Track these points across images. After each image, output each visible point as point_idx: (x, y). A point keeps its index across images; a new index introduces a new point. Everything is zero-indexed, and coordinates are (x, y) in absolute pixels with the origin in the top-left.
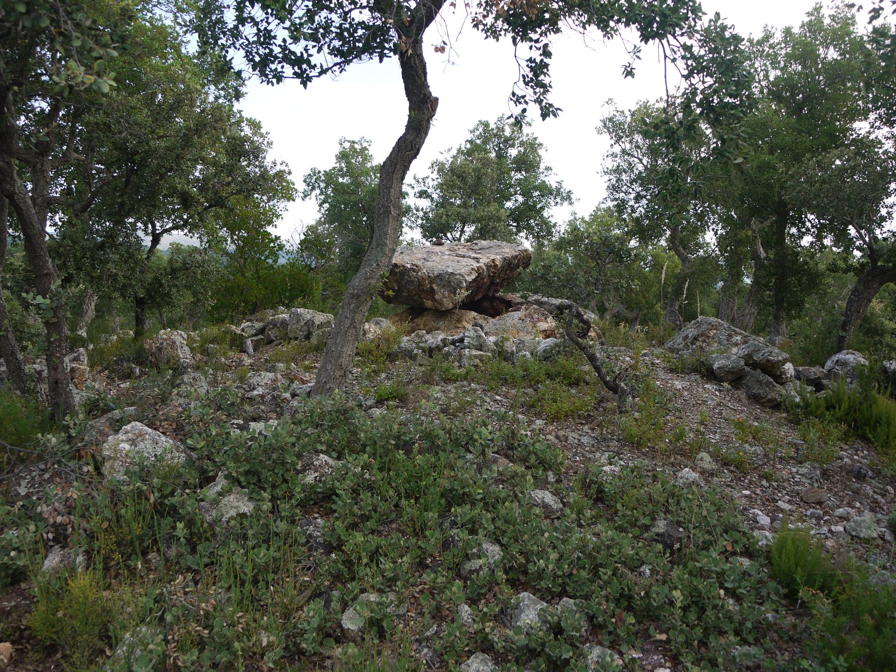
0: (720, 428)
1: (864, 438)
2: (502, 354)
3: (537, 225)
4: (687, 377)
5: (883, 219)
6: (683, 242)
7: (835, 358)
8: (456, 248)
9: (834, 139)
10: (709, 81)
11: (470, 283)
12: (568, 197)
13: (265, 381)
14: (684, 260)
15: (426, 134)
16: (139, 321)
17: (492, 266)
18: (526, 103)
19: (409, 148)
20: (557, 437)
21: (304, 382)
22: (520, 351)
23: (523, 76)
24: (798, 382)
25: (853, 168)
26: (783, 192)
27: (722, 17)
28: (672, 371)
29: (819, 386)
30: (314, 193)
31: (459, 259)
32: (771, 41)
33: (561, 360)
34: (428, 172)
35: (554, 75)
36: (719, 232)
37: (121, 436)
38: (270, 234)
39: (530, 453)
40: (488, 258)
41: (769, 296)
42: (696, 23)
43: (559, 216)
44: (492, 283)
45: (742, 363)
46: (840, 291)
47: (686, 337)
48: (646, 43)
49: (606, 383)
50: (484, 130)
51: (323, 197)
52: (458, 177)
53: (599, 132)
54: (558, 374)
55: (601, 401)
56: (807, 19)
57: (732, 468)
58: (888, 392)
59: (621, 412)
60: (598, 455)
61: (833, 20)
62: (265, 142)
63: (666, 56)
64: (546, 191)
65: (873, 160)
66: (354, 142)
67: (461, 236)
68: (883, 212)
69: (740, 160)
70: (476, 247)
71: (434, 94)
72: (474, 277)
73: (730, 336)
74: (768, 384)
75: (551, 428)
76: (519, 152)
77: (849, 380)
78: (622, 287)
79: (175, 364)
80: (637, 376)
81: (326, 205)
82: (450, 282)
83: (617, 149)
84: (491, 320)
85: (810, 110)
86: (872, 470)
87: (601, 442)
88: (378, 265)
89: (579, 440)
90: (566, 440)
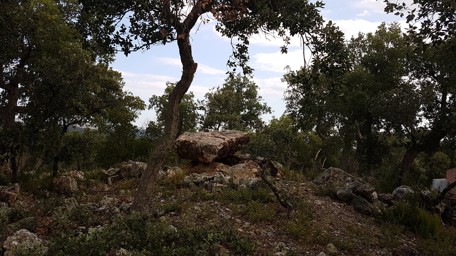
0: (340, 226)
1: (413, 231)
2: (233, 186)
3: (255, 122)
4: (324, 198)
5: (418, 122)
6: (323, 131)
7: (398, 189)
8: (215, 133)
9: (394, 84)
10: (326, 54)
11: (220, 150)
12: (269, 110)
13: (108, 202)
14: (323, 139)
15: (191, 81)
16: (55, 168)
17: (231, 142)
18: (235, 66)
19: (183, 87)
20: (255, 232)
21: (128, 202)
22: (241, 184)
23: (234, 53)
24: (379, 201)
25: (402, 98)
26: (369, 109)
27: (333, 23)
28: (316, 195)
29: (390, 204)
30: (154, 107)
31: (217, 137)
32: (362, 40)
33: (260, 189)
34: (204, 98)
35: (250, 53)
36: (339, 127)
37: (14, 238)
38: (132, 125)
39: (238, 244)
40: (229, 138)
41: (364, 157)
42: (319, 26)
43: (266, 118)
44: (231, 150)
45: (351, 192)
46: (399, 155)
47: (324, 177)
48: (293, 36)
49: (281, 203)
50: (231, 80)
51: (158, 108)
52: (217, 101)
53: (283, 81)
54: (258, 197)
55: (279, 212)
56: (378, 30)
57: (346, 252)
58: (424, 207)
59: (289, 218)
60: (276, 243)
61: (390, 30)
62: (121, 83)
63: (304, 43)
64: (259, 107)
65: (412, 94)
66: (173, 84)
67: (219, 127)
68: (417, 118)
69: (342, 95)
70: (224, 133)
71: (195, 62)
72: (222, 147)
73: (345, 177)
74: (365, 203)
75: (253, 227)
76: (247, 89)
77: (405, 201)
78: (289, 154)
79: (67, 191)
80: (298, 198)
81: (160, 112)
82: (210, 149)
83: (291, 88)
84: (230, 167)
85: (381, 71)
86: (418, 250)
87: (278, 235)
88: (166, 144)
89: (266, 234)
90: (260, 234)
